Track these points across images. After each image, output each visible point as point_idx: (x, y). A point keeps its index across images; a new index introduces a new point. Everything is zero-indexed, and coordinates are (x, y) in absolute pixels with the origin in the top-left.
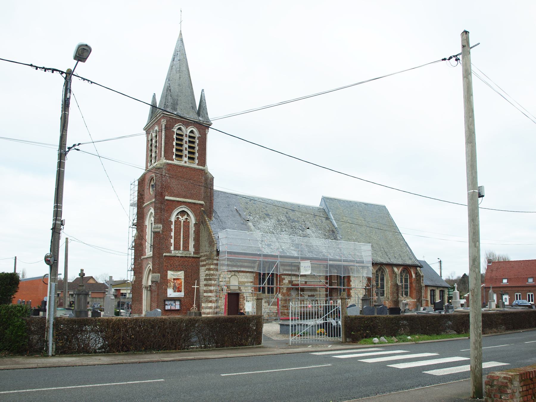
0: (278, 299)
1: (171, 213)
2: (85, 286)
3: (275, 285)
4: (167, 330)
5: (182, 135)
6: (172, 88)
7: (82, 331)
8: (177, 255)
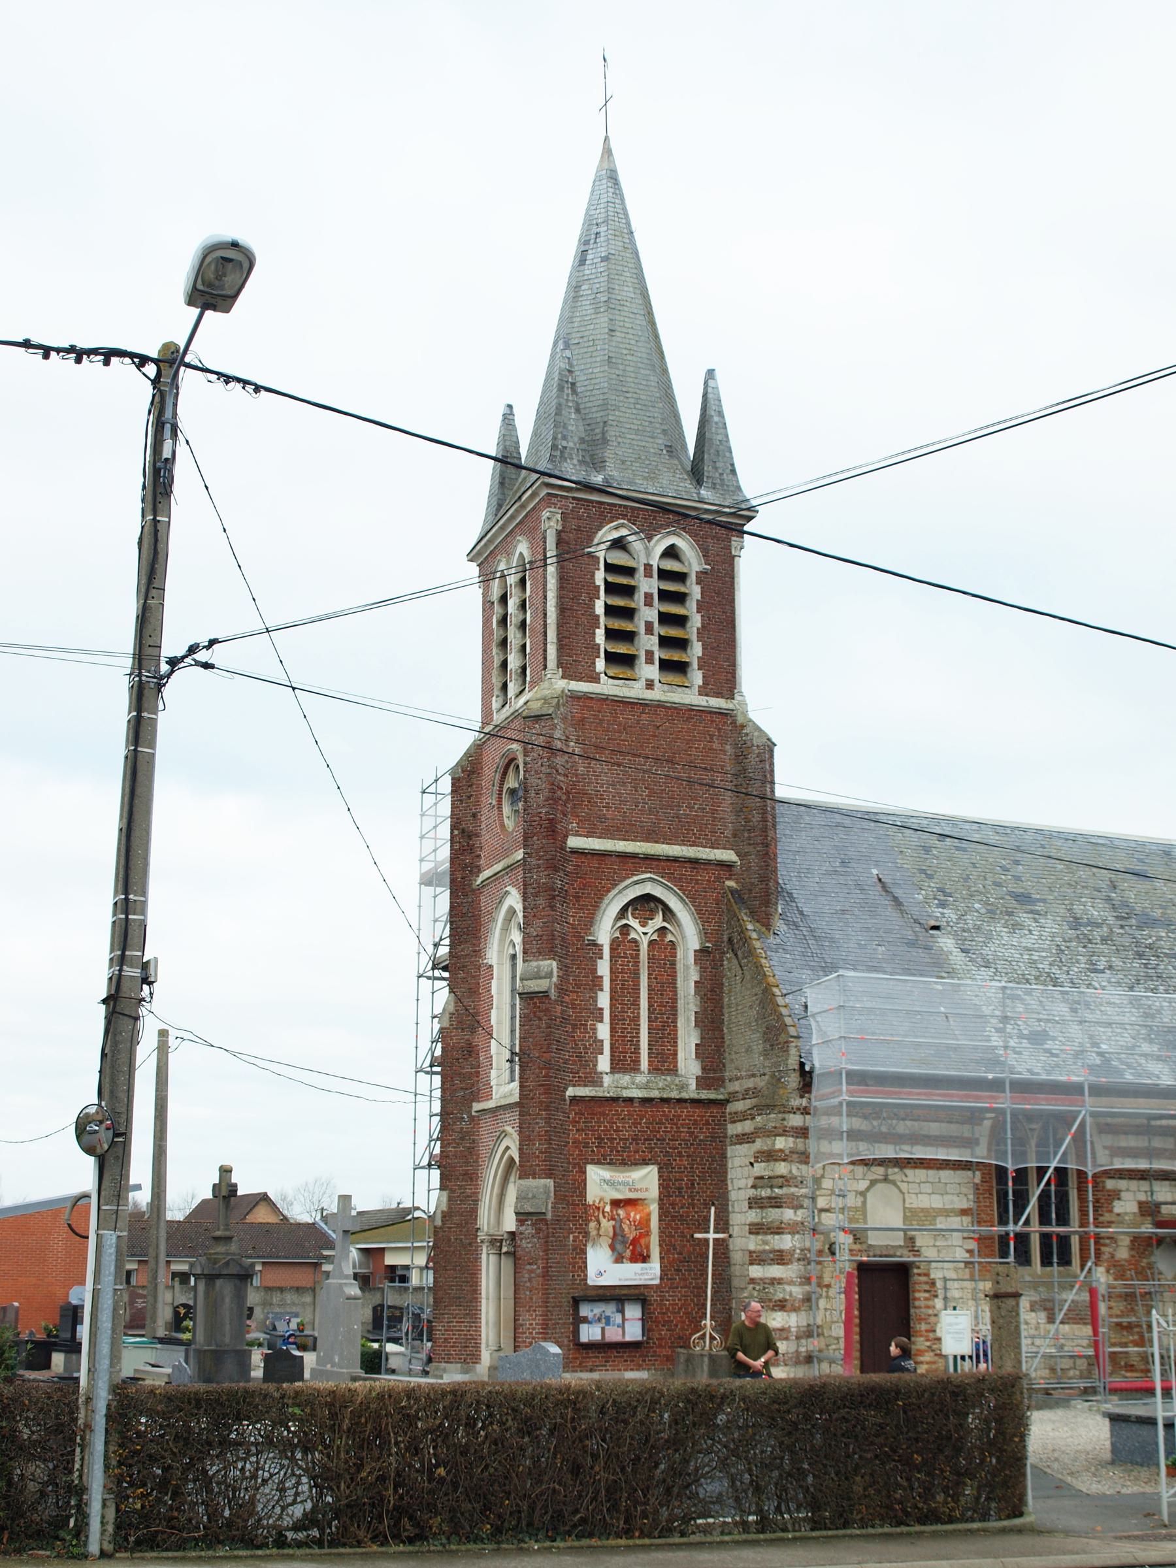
0: (1093, 1292)
1: (596, 906)
2: (238, 1238)
3: (1074, 1226)
4: (592, 1444)
5: (630, 571)
6: (581, 378)
7: (225, 1443)
8: (626, 1094)
